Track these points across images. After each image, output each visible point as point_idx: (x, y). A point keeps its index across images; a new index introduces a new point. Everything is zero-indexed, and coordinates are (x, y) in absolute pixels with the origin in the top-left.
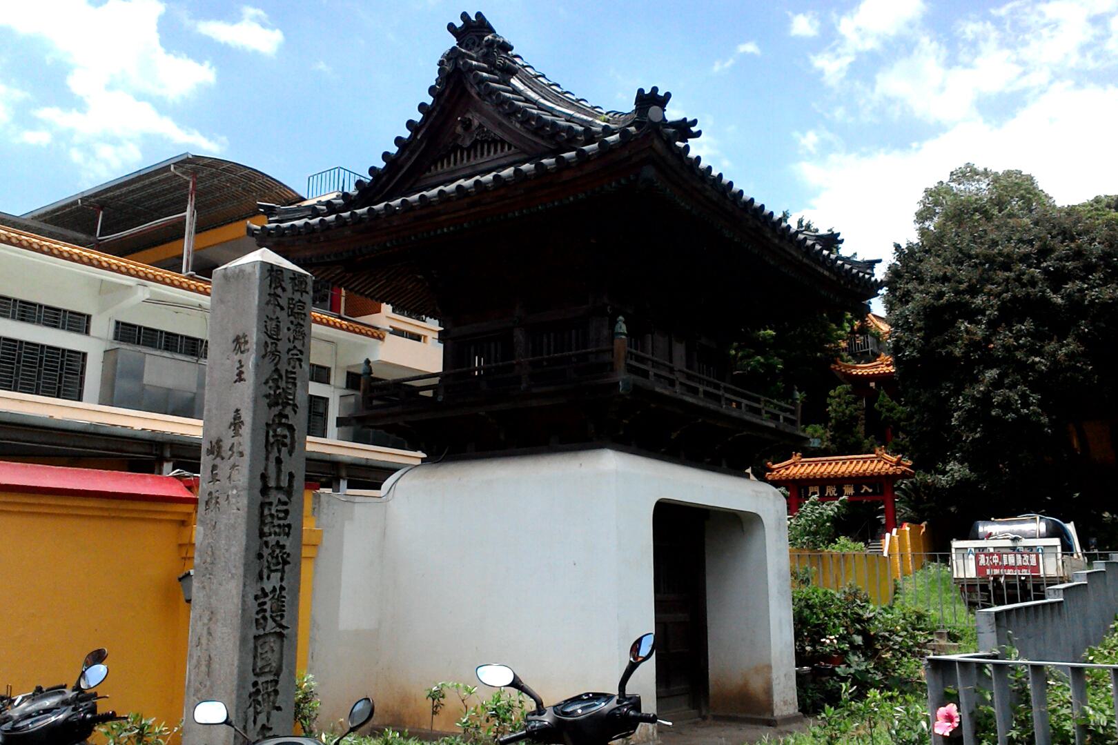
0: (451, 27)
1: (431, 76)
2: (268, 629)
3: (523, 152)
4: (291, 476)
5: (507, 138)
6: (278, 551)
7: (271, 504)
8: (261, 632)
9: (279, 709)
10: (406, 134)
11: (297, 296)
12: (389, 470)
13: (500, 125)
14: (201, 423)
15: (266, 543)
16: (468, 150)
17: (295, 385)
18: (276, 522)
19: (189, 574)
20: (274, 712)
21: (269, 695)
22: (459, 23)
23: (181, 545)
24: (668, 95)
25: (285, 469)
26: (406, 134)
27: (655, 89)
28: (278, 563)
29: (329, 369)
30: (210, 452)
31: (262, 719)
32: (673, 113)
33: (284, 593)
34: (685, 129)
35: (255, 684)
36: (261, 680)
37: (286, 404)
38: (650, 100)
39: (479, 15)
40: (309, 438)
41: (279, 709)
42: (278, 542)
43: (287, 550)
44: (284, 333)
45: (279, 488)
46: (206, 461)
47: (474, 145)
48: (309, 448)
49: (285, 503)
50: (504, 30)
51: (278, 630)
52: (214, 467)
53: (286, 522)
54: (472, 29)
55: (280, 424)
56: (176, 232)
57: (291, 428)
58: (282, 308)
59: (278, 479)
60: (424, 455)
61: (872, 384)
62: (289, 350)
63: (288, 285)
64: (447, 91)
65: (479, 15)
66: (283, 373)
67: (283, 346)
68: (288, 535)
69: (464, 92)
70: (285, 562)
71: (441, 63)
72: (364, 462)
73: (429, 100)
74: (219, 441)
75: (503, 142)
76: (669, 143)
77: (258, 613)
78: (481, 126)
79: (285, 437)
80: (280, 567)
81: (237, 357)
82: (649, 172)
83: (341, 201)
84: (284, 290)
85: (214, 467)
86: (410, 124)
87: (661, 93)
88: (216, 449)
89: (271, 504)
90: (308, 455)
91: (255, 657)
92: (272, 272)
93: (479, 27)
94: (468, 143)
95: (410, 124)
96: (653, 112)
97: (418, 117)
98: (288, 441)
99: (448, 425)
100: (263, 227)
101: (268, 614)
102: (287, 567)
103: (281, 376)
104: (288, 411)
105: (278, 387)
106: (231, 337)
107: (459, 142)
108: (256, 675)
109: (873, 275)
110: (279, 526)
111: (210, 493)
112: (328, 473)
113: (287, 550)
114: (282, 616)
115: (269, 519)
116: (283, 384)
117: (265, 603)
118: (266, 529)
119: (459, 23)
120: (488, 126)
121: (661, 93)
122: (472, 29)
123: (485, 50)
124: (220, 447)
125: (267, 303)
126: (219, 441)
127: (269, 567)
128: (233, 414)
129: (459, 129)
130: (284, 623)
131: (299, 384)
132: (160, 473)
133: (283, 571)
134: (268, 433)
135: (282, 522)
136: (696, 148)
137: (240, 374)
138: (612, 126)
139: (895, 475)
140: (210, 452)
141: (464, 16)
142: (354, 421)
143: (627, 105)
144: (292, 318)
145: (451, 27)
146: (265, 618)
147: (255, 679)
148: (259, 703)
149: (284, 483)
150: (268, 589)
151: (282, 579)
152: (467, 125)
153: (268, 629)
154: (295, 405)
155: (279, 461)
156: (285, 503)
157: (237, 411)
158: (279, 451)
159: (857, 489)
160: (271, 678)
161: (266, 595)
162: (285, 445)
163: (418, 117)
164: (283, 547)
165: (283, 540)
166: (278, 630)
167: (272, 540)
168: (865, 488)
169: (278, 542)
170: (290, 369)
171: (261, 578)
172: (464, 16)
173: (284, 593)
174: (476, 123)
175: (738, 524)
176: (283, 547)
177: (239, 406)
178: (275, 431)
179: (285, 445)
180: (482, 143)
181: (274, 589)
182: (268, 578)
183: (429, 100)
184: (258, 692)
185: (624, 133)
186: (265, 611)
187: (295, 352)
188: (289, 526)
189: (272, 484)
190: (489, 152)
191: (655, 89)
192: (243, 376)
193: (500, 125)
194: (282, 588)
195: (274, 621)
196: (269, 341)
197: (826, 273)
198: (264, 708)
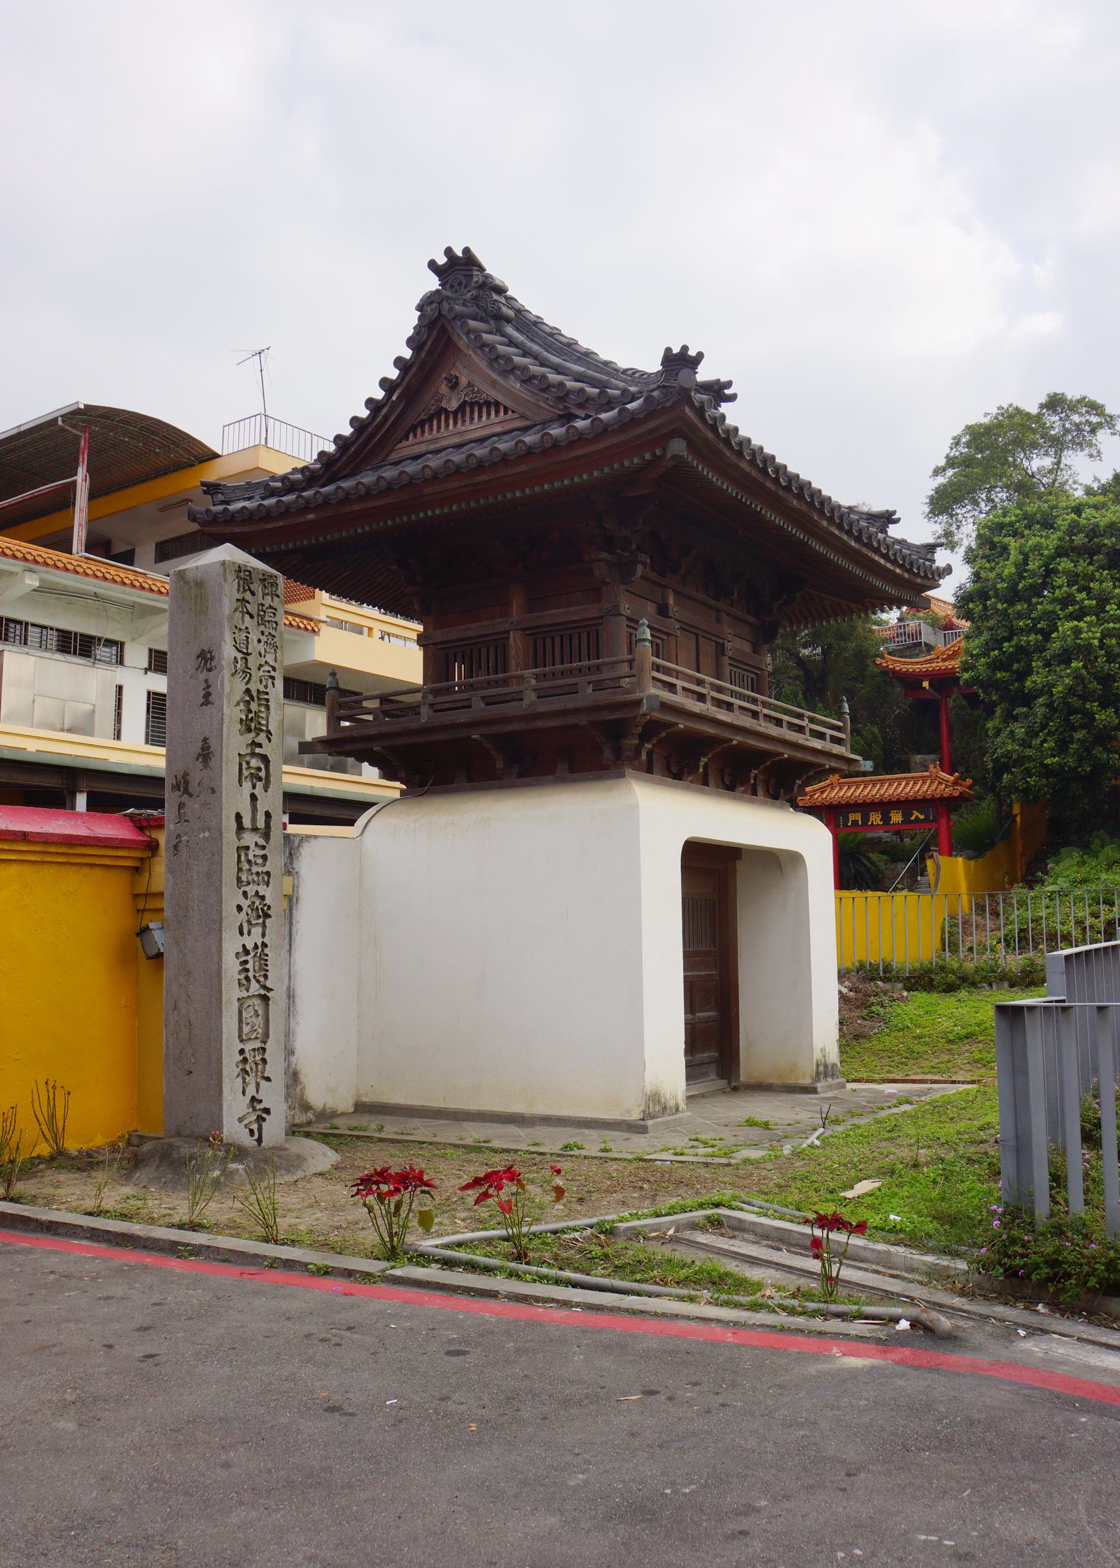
0: (432, 265)
1: (411, 320)
2: (252, 991)
3: (523, 417)
4: (268, 815)
5: (501, 399)
6: (257, 903)
7: (247, 848)
8: (245, 994)
9: (268, 1079)
10: (379, 394)
11: (268, 601)
12: (363, 806)
13: (494, 384)
14: (162, 750)
15: (245, 894)
16: (455, 413)
17: (268, 707)
18: (255, 869)
19: (148, 928)
20: (263, 1083)
21: (257, 1064)
22: (442, 260)
23: (136, 896)
24: (700, 356)
25: (262, 807)
26: (379, 394)
27: (685, 348)
28: (259, 917)
29: (166, 653)
30: (176, 787)
31: (251, 1091)
32: (704, 374)
33: (266, 951)
34: (719, 391)
35: (242, 1052)
36: (248, 1047)
37: (259, 730)
38: (680, 362)
39: (467, 251)
40: (286, 768)
41: (268, 1079)
42: (257, 892)
43: (268, 901)
44: (254, 647)
45: (255, 829)
46: (170, 797)
47: (462, 407)
48: (287, 779)
49: (263, 848)
50: (494, 266)
51: (263, 992)
52: (181, 806)
53: (265, 869)
54: (459, 270)
55: (253, 754)
56: (65, 500)
57: (265, 759)
58: (252, 617)
59: (254, 819)
60: (404, 787)
61: (926, 684)
62: (261, 666)
63: (257, 587)
64: (429, 343)
65: (467, 251)
66: (255, 694)
67: (253, 662)
68: (268, 884)
69: (450, 342)
70: (267, 916)
71: (420, 308)
72: (308, 792)
73: (407, 353)
74: (186, 775)
75: (497, 404)
76: (700, 411)
77: (240, 972)
78: (470, 385)
79: (259, 769)
80: (261, 921)
81: (202, 676)
82: (678, 447)
83: (299, 476)
84: (253, 593)
85: (181, 806)
86: (384, 383)
87: (692, 352)
88: (183, 785)
89: (247, 848)
90: (287, 790)
91: (240, 1021)
92: (244, 576)
93: (466, 264)
94: (454, 405)
95: (384, 383)
96: (684, 373)
97: (394, 374)
98: (262, 774)
99: (436, 751)
100: (208, 511)
101: (251, 974)
102: (268, 921)
103: (252, 698)
104: (262, 738)
105: (250, 711)
106: (196, 651)
107: (444, 404)
108: (242, 1041)
109: (933, 561)
110: (258, 873)
111: (178, 836)
112: (308, 808)
113: (268, 901)
114: (266, 977)
115: (246, 866)
116: (254, 706)
117: (246, 962)
118: (244, 878)
119: (442, 260)
120: (480, 384)
121: (692, 352)
122: (459, 270)
123: (474, 292)
124: (187, 783)
125: (236, 610)
126: (186, 775)
127: (249, 922)
128: (200, 744)
129: (444, 388)
130: (268, 984)
131: (272, 704)
132: (73, 807)
133: (264, 925)
134: (240, 765)
135: (260, 869)
136: (731, 414)
137: (207, 695)
138: (632, 389)
139: (951, 798)
140: (176, 787)
141: (449, 252)
142: (319, 747)
143: (652, 364)
144: (262, 628)
145: (432, 265)
146: (247, 979)
147: (241, 1046)
148: (247, 1072)
149: (261, 824)
150: (250, 947)
151: (263, 935)
152: (454, 384)
153: (252, 991)
154: (269, 732)
155: (253, 798)
156: (263, 848)
157: (205, 740)
158: (254, 787)
159: (906, 816)
160: (258, 1044)
161: (246, 952)
162: (260, 779)
163: (394, 374)
164: (263, 898)
165: (262, 889)
166: (263, 992)
167: (251, 889)
168: (916, 813)
169: (257, 892)
170: (262, 689)
171: (242, 934)
172: (449, 252)
173: (266, 951)
174: (464, 381)
175: (780, 864)
176: (263, 898)
177: (208, 734)
178: (248, 763)
179: (260, 779)
180: (472, 405)
181: (256, 947)
182: (249, 933)
183: (407, 353)
184: (245, 1060)
185: (649, 400)
186: (247, 970)
187: (267, 668)
188: (268, 873)
189: (247, 823)
190: (480, 417)
191: (685, 348)
192: (211, 699)
193: (494, 384)
194: (264, 945)
195: (258, 981)
196: (239, 656)
197: (882, 561)
198: (251, 1079)
